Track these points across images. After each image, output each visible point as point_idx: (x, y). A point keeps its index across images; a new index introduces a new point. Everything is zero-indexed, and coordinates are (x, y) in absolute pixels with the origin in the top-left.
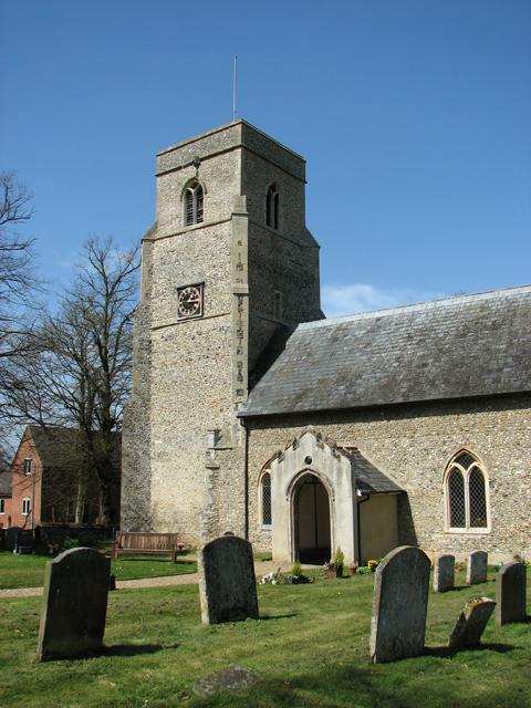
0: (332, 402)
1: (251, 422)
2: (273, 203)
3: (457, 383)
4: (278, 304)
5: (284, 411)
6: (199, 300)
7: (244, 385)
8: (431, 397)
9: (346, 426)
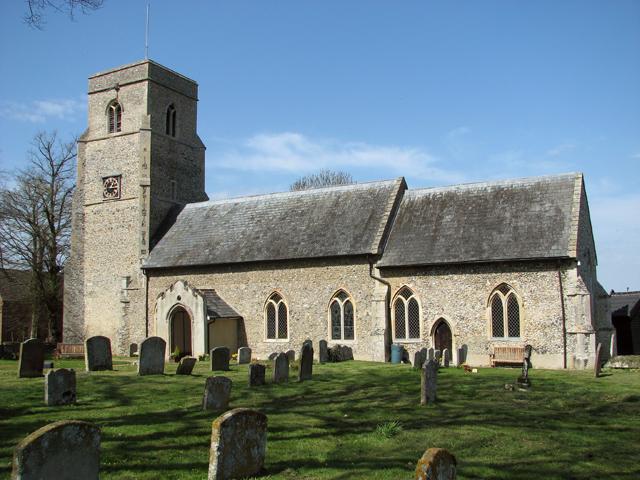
0: (199, 261)
1: (150, 272)
2: (171, 118)
3: (273, 251)
4: (173, 190)
6: (118, 187)
8: (257, 259)
9: (208, 276)
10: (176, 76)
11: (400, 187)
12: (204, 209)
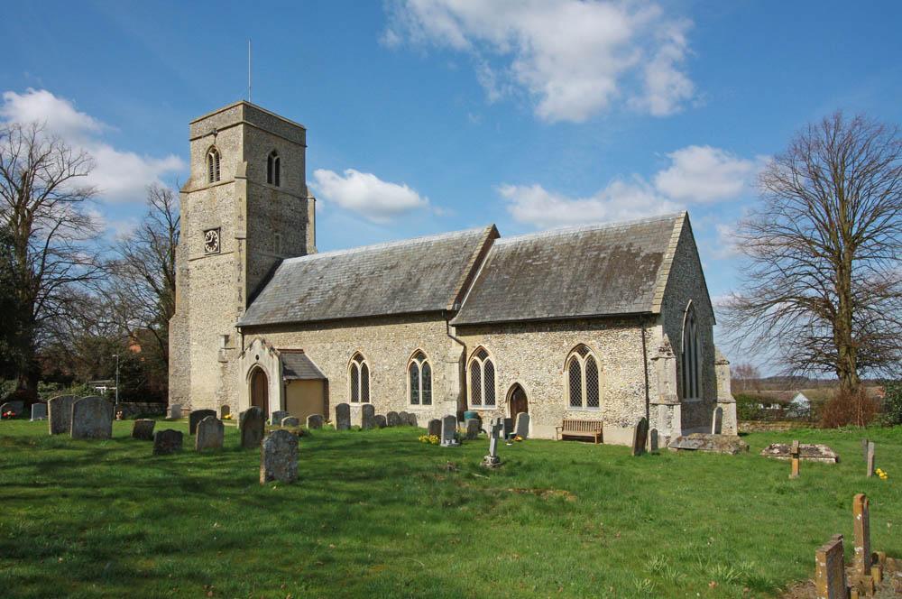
1: (246, 330)
2: (274, 165)
4: (277, 244)
5: (262, 323)
7: (243, 304)
10: (279, 121)
11: (489, 236)
12: (304, 263)
